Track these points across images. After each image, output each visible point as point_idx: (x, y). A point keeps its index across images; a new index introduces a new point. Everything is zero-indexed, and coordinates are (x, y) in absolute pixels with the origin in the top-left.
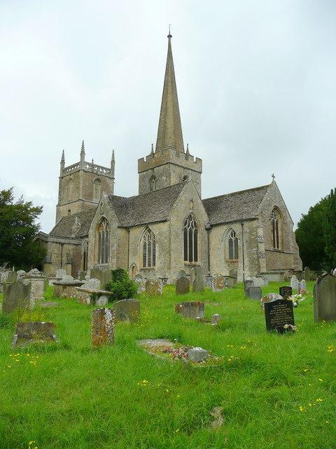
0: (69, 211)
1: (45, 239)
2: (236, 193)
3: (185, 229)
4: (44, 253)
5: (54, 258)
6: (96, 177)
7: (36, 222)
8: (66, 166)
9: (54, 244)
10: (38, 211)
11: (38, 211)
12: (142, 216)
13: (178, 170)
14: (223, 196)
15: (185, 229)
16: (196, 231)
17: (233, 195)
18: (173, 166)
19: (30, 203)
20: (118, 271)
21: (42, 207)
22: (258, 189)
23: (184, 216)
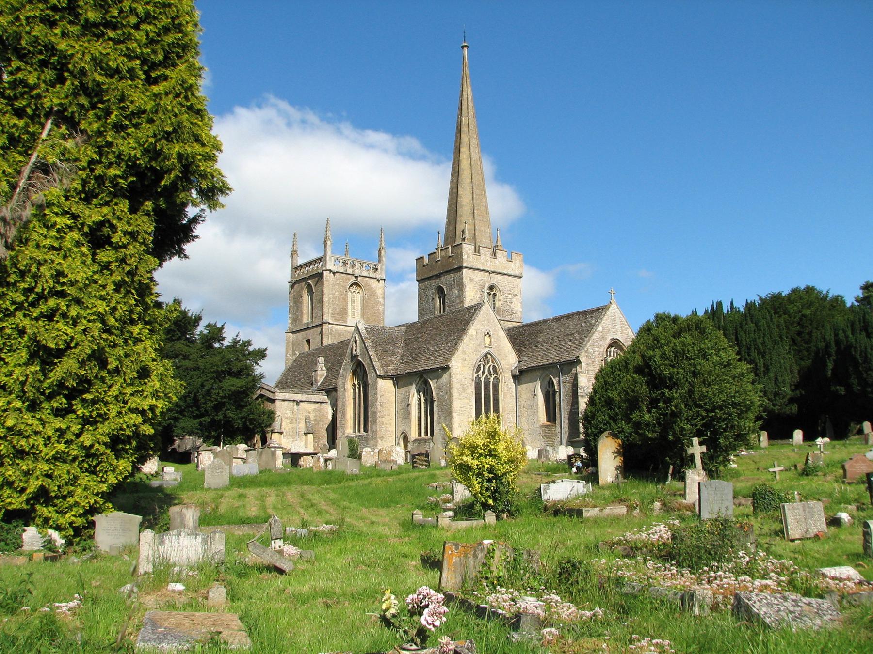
0: (308, 341)
1: (271, 396)
2: (563, 317)
3: (478, 378)
4: (271, 415)
5: (286, 426)
6: (353, 279)
7: (258, 370)
8: (300, 261)
9: (286, 403)
10: (261, 354)
11: (261, 354)
12: (415, 359)
13: (479, 276)
14: (545, 321)
15: (366, 430)
16: (497, 379)
17: (558, 319)
18: (470, 271)
19: (221, 151)
20: (170, 495)
21: (266, 349)
22: (585, 313)
23: (475, 358)
